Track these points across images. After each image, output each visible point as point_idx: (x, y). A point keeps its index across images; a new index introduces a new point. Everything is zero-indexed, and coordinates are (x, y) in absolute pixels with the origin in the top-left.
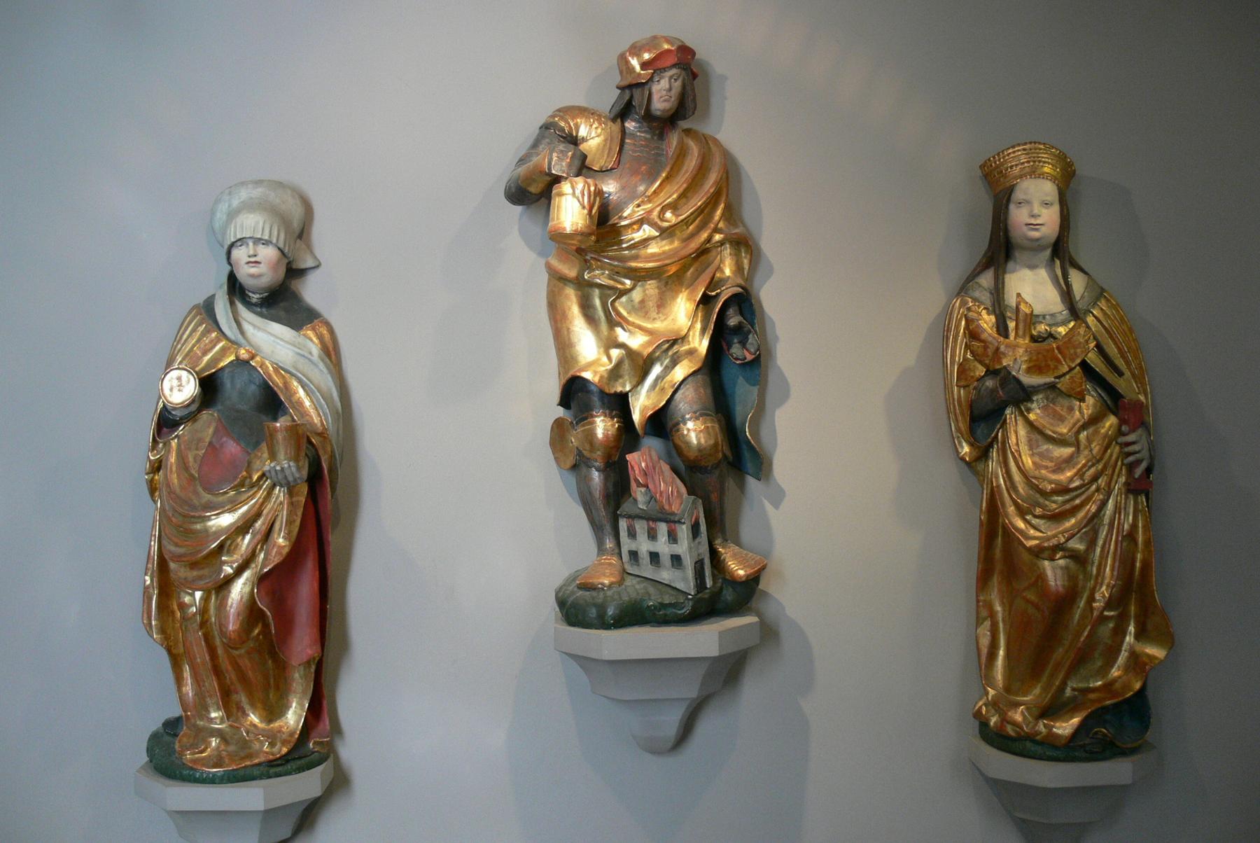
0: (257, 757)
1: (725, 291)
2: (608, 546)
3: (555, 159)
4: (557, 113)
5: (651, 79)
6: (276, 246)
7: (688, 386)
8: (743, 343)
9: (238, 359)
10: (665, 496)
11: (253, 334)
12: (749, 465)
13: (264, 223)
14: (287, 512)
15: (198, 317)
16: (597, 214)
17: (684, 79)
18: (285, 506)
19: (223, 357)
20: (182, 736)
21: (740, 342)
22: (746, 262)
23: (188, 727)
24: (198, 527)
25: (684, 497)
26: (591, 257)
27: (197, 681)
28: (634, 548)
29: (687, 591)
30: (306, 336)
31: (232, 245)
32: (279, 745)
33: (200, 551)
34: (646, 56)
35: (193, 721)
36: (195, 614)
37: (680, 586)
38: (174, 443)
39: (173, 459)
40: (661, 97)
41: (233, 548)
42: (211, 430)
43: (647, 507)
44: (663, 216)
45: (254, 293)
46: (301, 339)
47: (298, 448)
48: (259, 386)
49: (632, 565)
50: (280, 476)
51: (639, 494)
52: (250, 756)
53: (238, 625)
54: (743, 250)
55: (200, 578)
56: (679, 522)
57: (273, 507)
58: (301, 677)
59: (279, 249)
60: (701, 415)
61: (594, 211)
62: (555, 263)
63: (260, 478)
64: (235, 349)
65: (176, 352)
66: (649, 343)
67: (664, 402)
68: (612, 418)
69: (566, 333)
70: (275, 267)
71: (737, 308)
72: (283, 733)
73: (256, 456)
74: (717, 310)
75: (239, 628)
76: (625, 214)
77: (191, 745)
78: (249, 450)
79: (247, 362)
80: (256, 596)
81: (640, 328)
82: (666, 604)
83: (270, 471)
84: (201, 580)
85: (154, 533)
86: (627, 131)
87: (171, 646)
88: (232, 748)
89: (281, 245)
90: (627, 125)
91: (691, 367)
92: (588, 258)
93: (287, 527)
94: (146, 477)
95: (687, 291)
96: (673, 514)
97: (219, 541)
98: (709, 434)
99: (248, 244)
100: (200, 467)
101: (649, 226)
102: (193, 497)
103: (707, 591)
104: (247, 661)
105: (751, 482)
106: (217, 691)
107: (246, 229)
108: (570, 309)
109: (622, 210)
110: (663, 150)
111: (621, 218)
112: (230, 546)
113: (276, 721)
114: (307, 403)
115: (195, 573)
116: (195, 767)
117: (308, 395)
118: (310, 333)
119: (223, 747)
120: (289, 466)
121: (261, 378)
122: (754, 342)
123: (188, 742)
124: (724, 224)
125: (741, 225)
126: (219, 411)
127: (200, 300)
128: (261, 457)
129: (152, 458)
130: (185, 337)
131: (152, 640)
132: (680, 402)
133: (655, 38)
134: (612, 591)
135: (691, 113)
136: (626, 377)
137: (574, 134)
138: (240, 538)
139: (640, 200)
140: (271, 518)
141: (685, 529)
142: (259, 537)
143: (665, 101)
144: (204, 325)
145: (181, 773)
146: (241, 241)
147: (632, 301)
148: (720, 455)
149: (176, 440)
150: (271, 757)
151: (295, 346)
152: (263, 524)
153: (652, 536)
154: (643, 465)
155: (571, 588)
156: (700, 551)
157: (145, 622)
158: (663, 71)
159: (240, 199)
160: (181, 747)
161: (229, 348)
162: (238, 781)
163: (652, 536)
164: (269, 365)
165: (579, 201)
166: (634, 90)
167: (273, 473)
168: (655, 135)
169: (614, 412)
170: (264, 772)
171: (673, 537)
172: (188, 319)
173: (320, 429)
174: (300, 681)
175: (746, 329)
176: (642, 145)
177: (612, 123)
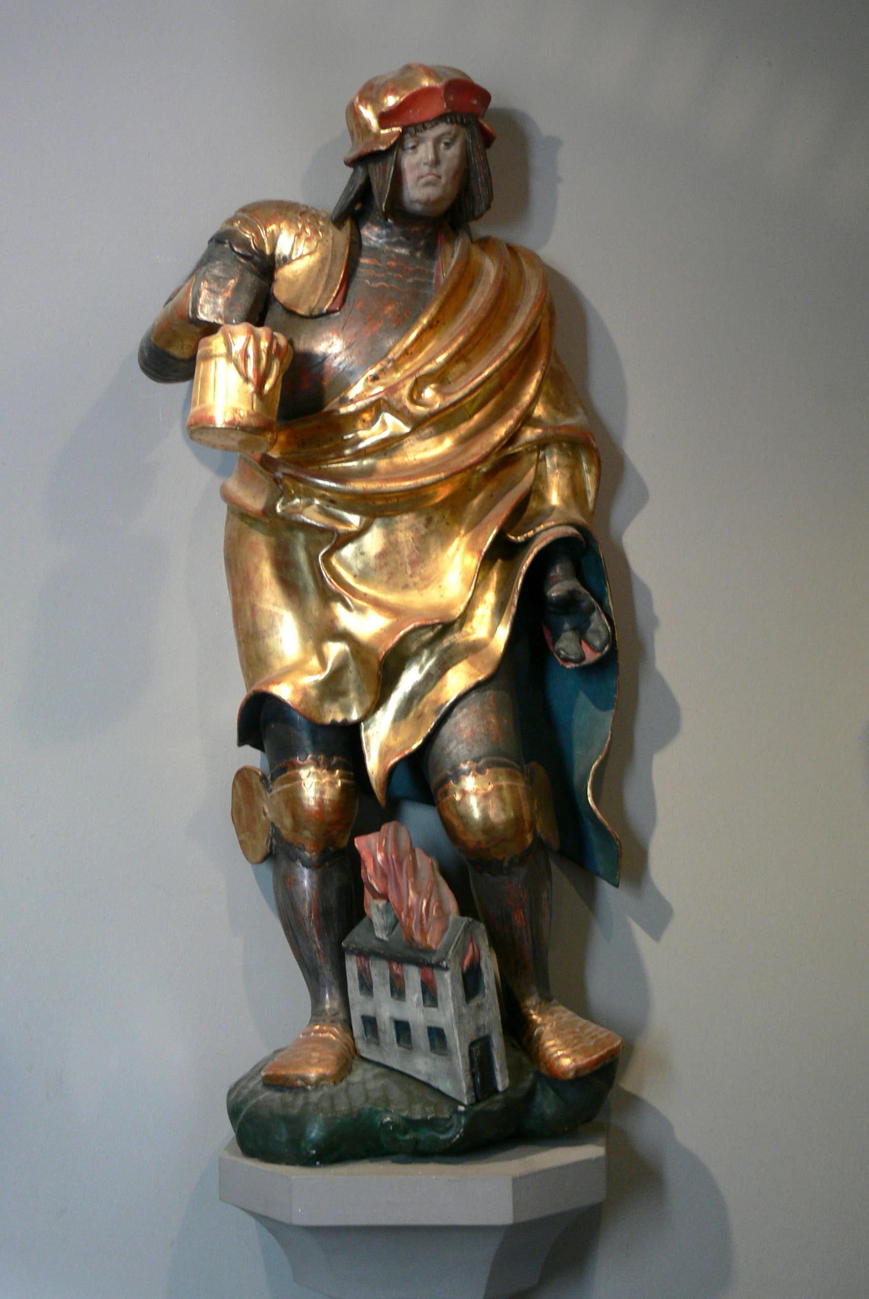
1: (544, 534)
2: (327, 1006)
3: (204, 293)
4: (240, 214)
5: (399, 144)
7: (465, 711)
8: (581, 631)
10: (415, 917)
12: (599, 860)
16: (278, 392)
17: (465, 145)
21: (574, 629)
22: (589, 480)
25: (451, 918)
26: (284, 474)
28: (369, 1012)
29: (458, 1098)
34: (391, 101)
37: (446, 1086)
40: (421, 177)
43: (388, 936)
44: (419, 396)
49: (368, 1042)
51: (374, 908)
54: (583, 458)
56: (438, 966)
60: (490, 765)
61: (267, 387)
62: (233, 485)
66: (392, 630)
67: (420, 742)
68: (331, 769)
69: (249, 613)
71: (568, 565)
74: (524, 568)
76: (352, 394)
81: (377, 604)
82: (418, 1121)
86: (365, 243)
90: (365, 232)
91: (471, 675)
92: (279, 475)
95: (469, 535)
96: (428, 950)
98: (502, 799)
101: (392, 414)
103: (499, 1097)
105: (605, 888)
108: (257, 568)
109: (348, 387)
110: (431, 278)
111: (345, 401)
122: (601, 629)
124: (545, 409)
125: (580, 410)
132: (450, 741)
133: (408, 68)
134: (320, 1093)
135: (483, 206)
136: (352, 695)
137: (268, 252)
139: (378, 367)
141: (449, 981)
143: (428, 184)
147: (362, 554)
148: (529, 838)
153: (398, 990)
154: (379, 857)
155: (252, 1085)
156: (481, 1022)
158: (420, 127)
163: (398, 990)
165: (237, 367)
166: (371, 166)
168: (418, 250)
169: (335, 760)
171: (430, 995)
175: (585, 604)
176: (390, 268)
177: (336, 230)
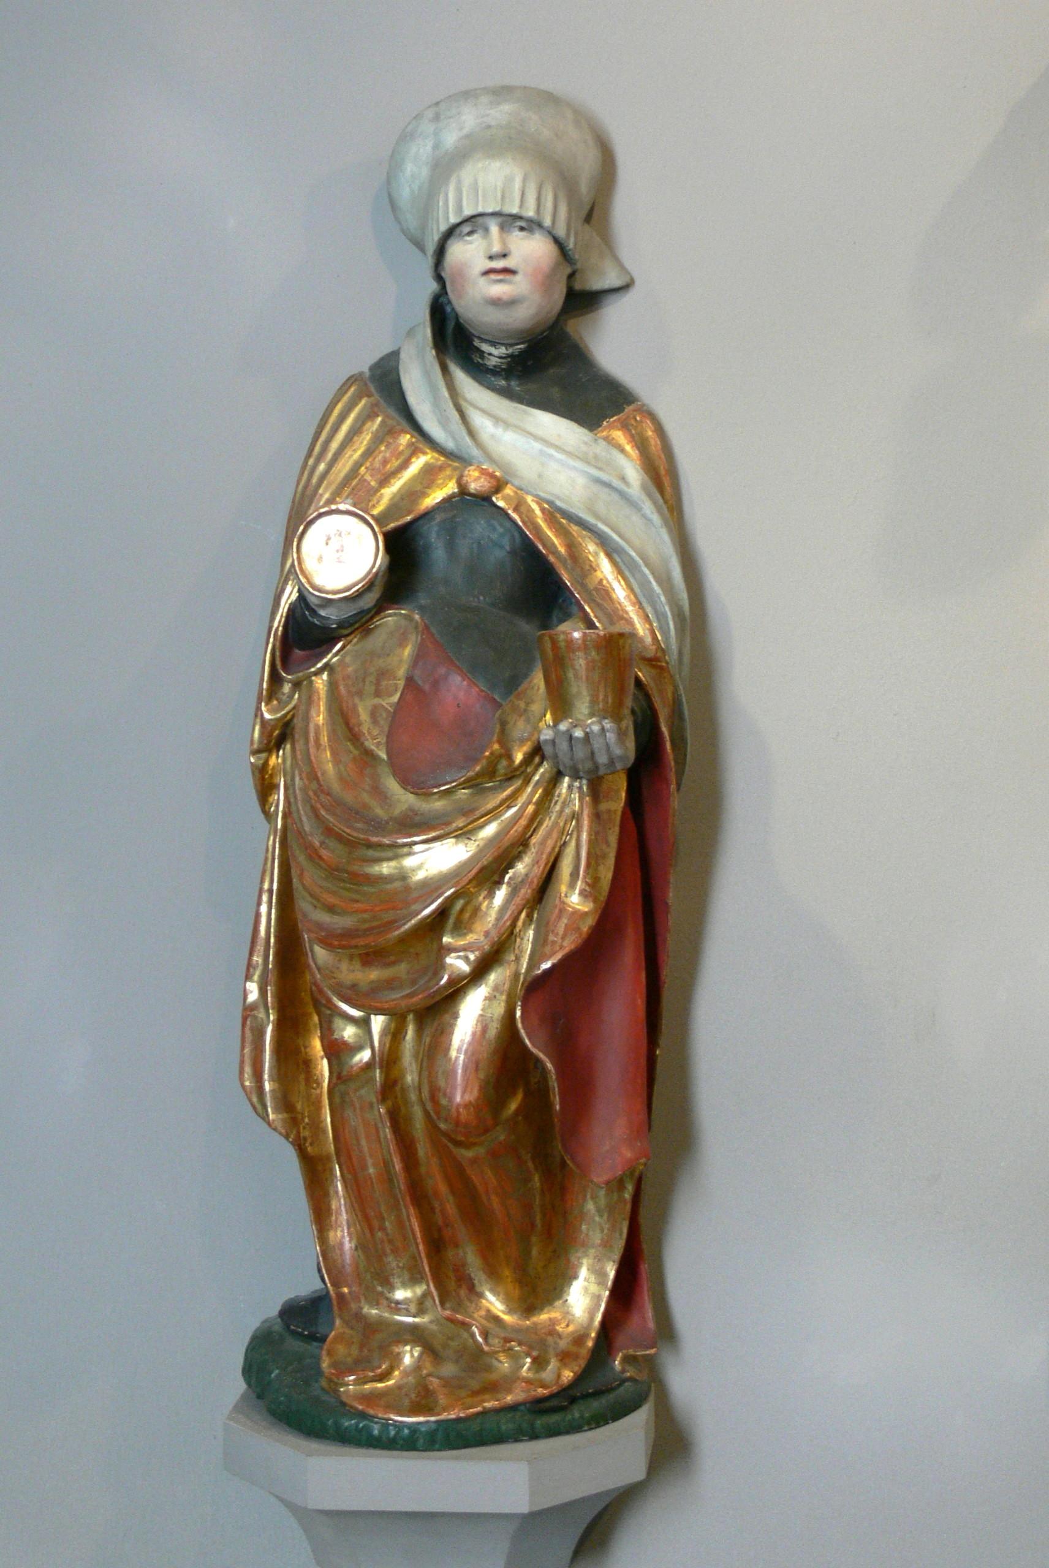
0: (509, 1391)
6: (550, 233)
9: (463, 491)
11: (493, 436)
13: (525, 180)
14: (590, 834)
15: (363, 402)
18: (586, 823)
19: (429, 487)
20: (335, 1338)
23: (346, 1323)
24: (386, 868)
27: (366, 1217)
30: (610, 441)
31: (450, 233)
32: (553, 1364)
33: (391, 924)
35: (353, 1306)
36: (369, 1066)
38: (321, 682)
39: (320, 717)
41: (467, 915)
42: (407, 652)
45: (493, 344)
46: (600, 448)
47: (620, 691)
48: (513, 552)
50: (580, 753)
52: (492, 1388)
53: (476, 1093)
55: (390, 984)
57: (556, 823)
58: (599, 1211)
59: (557, 241)
63: (528, 760)
64: (455, 469)
65: (314, 480)
70: (546, 283)
72: (560, 1336)
73: (515, 708)
75: (478, 1098)
77: (357, 1362)
78: (496, 697)
79: (484, 499)
80: (520, 1025)
83: (553, 742)
84: (392, 989)
85: (266, 886)
87: (305, 1139)
88: (449, 1369)
89: (561, 232)
93: (591, 871)
94: (252, 760)
97: (440, 900)
99: (487, 230)
100: (389, 736)
102: (373, 803)
104: (489, 1173)
106: (419, 1240)
107: (484, 196)
112: (462, 911)
113: (542, 1310)
114: (620, 592)
115: (374, 974)
116: (371, 1412)
117: (620, 572)
118: (619, 435)
119: (428, 1367)
120: (603, 729)
121: (517, 535)
123: (350, 1355)
126: (422, 609)
127: (363, 362)
128: (525, 710)
129: (267, 716)
130: (334, 445)
131: (265, 1125)
138: (484, 893)
140: (553, 848)
142: (526, 892)
144: (380, 419)
145: (336, 1423)
146: (473, 223)
149: (325, 676)
150: (541, 1392)
151: (587, 462)
152: (536, 862)
157: (247, 1083)
159: (461, 129)
160: (334, 1365)
161: (441, 468)
162: (467, 1446)
164: (535, 507)
167: (564, 746)
170: (525, 1426)
172: (339, 407)
173: (651, 652)
174: (597, 1219)
